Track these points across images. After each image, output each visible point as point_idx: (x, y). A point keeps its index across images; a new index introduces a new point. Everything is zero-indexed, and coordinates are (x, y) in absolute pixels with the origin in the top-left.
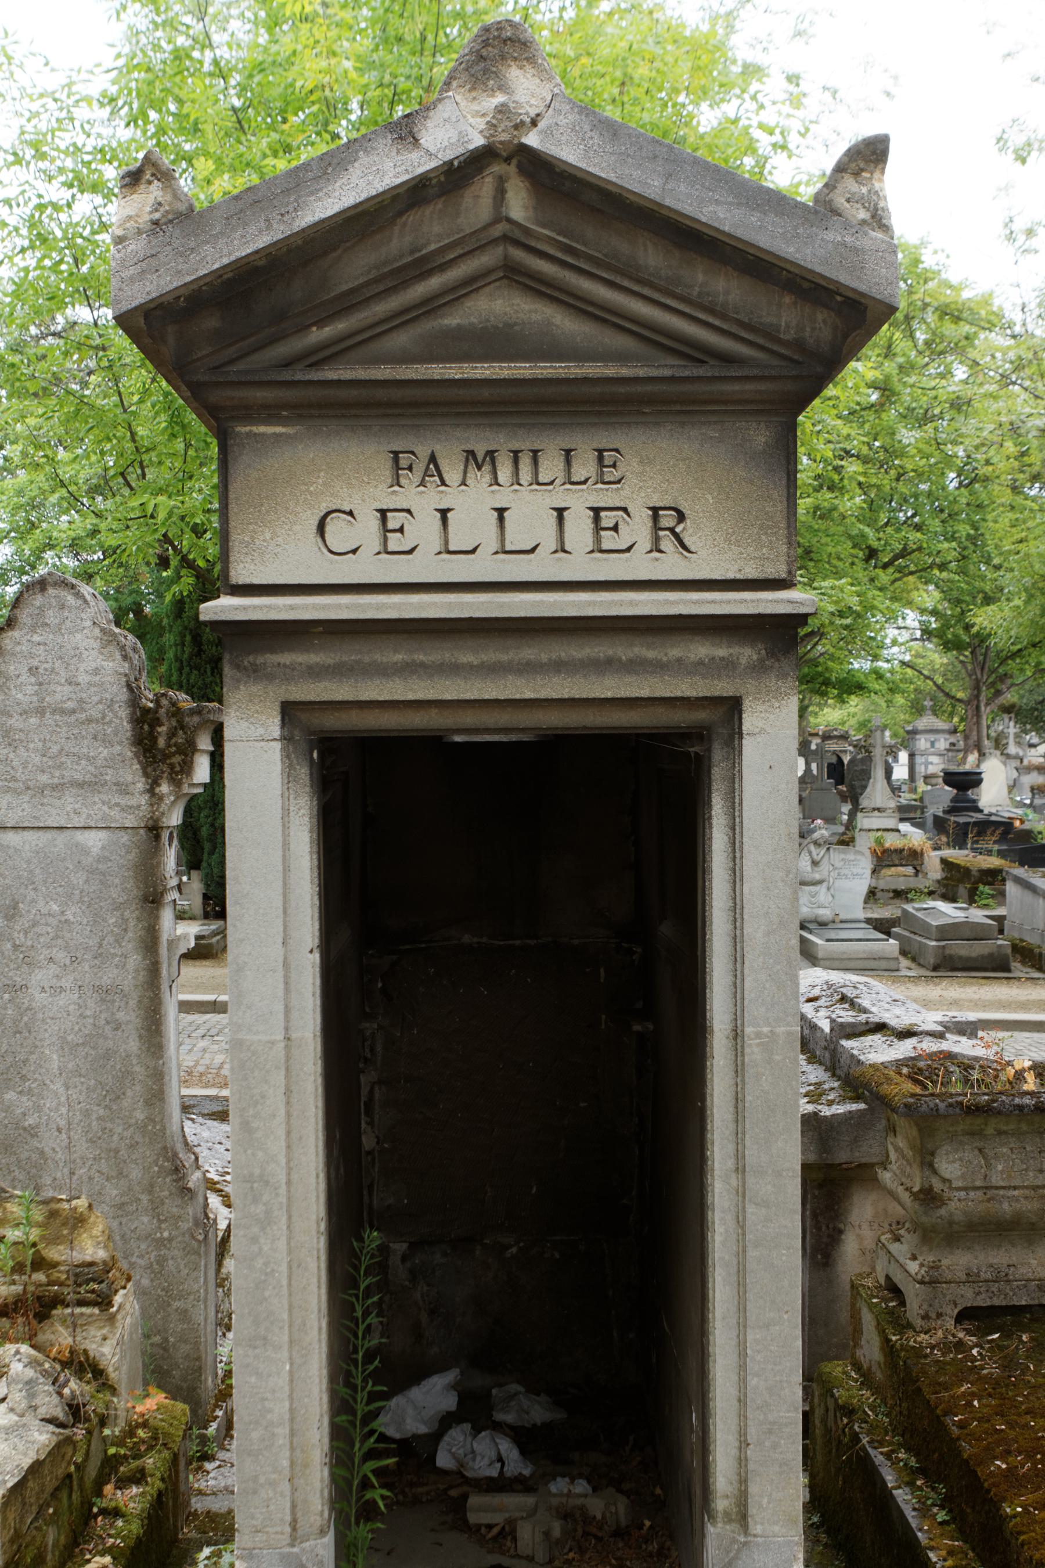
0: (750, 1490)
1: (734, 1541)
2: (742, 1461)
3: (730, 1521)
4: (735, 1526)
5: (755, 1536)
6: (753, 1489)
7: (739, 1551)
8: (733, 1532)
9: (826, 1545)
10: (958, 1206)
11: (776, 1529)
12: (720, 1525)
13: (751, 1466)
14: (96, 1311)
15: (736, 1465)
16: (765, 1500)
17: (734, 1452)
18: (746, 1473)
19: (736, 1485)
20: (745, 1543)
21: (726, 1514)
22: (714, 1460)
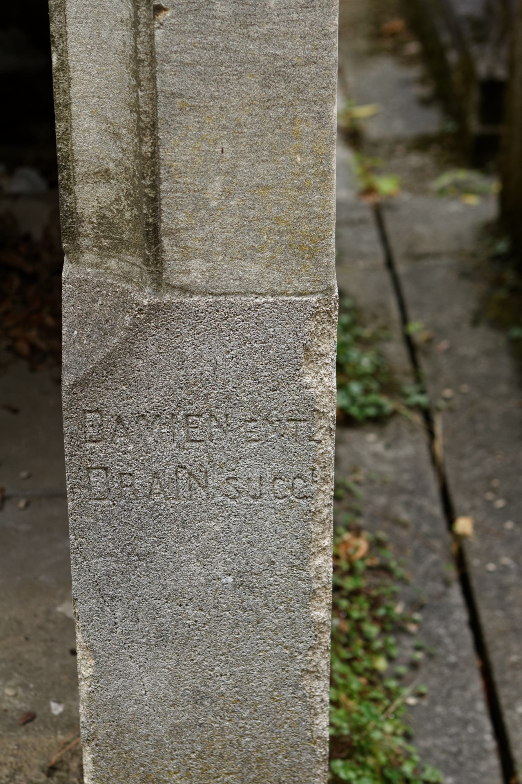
0: (165, 154)
1: (123, 303)
2: (143, 64)
3: (118, 246)
4: (130, 262)
5: (184, 290)
6: (176, 152)
7: (135, 331)
8: (127, 278)
9: (513, 290)
10: (312, 662)
11: (252, 270)
12: (88, 257)
13: (168, 80)
14: (96, 171)
15: (128, 79)
16: (216, 186)
17: (120, 37)
18: (154, 99)
19: (128, 137)
20: (155, 310)
21: (106, 224)
22: (64, 67)
